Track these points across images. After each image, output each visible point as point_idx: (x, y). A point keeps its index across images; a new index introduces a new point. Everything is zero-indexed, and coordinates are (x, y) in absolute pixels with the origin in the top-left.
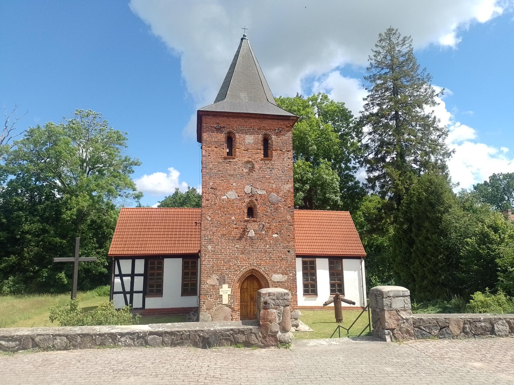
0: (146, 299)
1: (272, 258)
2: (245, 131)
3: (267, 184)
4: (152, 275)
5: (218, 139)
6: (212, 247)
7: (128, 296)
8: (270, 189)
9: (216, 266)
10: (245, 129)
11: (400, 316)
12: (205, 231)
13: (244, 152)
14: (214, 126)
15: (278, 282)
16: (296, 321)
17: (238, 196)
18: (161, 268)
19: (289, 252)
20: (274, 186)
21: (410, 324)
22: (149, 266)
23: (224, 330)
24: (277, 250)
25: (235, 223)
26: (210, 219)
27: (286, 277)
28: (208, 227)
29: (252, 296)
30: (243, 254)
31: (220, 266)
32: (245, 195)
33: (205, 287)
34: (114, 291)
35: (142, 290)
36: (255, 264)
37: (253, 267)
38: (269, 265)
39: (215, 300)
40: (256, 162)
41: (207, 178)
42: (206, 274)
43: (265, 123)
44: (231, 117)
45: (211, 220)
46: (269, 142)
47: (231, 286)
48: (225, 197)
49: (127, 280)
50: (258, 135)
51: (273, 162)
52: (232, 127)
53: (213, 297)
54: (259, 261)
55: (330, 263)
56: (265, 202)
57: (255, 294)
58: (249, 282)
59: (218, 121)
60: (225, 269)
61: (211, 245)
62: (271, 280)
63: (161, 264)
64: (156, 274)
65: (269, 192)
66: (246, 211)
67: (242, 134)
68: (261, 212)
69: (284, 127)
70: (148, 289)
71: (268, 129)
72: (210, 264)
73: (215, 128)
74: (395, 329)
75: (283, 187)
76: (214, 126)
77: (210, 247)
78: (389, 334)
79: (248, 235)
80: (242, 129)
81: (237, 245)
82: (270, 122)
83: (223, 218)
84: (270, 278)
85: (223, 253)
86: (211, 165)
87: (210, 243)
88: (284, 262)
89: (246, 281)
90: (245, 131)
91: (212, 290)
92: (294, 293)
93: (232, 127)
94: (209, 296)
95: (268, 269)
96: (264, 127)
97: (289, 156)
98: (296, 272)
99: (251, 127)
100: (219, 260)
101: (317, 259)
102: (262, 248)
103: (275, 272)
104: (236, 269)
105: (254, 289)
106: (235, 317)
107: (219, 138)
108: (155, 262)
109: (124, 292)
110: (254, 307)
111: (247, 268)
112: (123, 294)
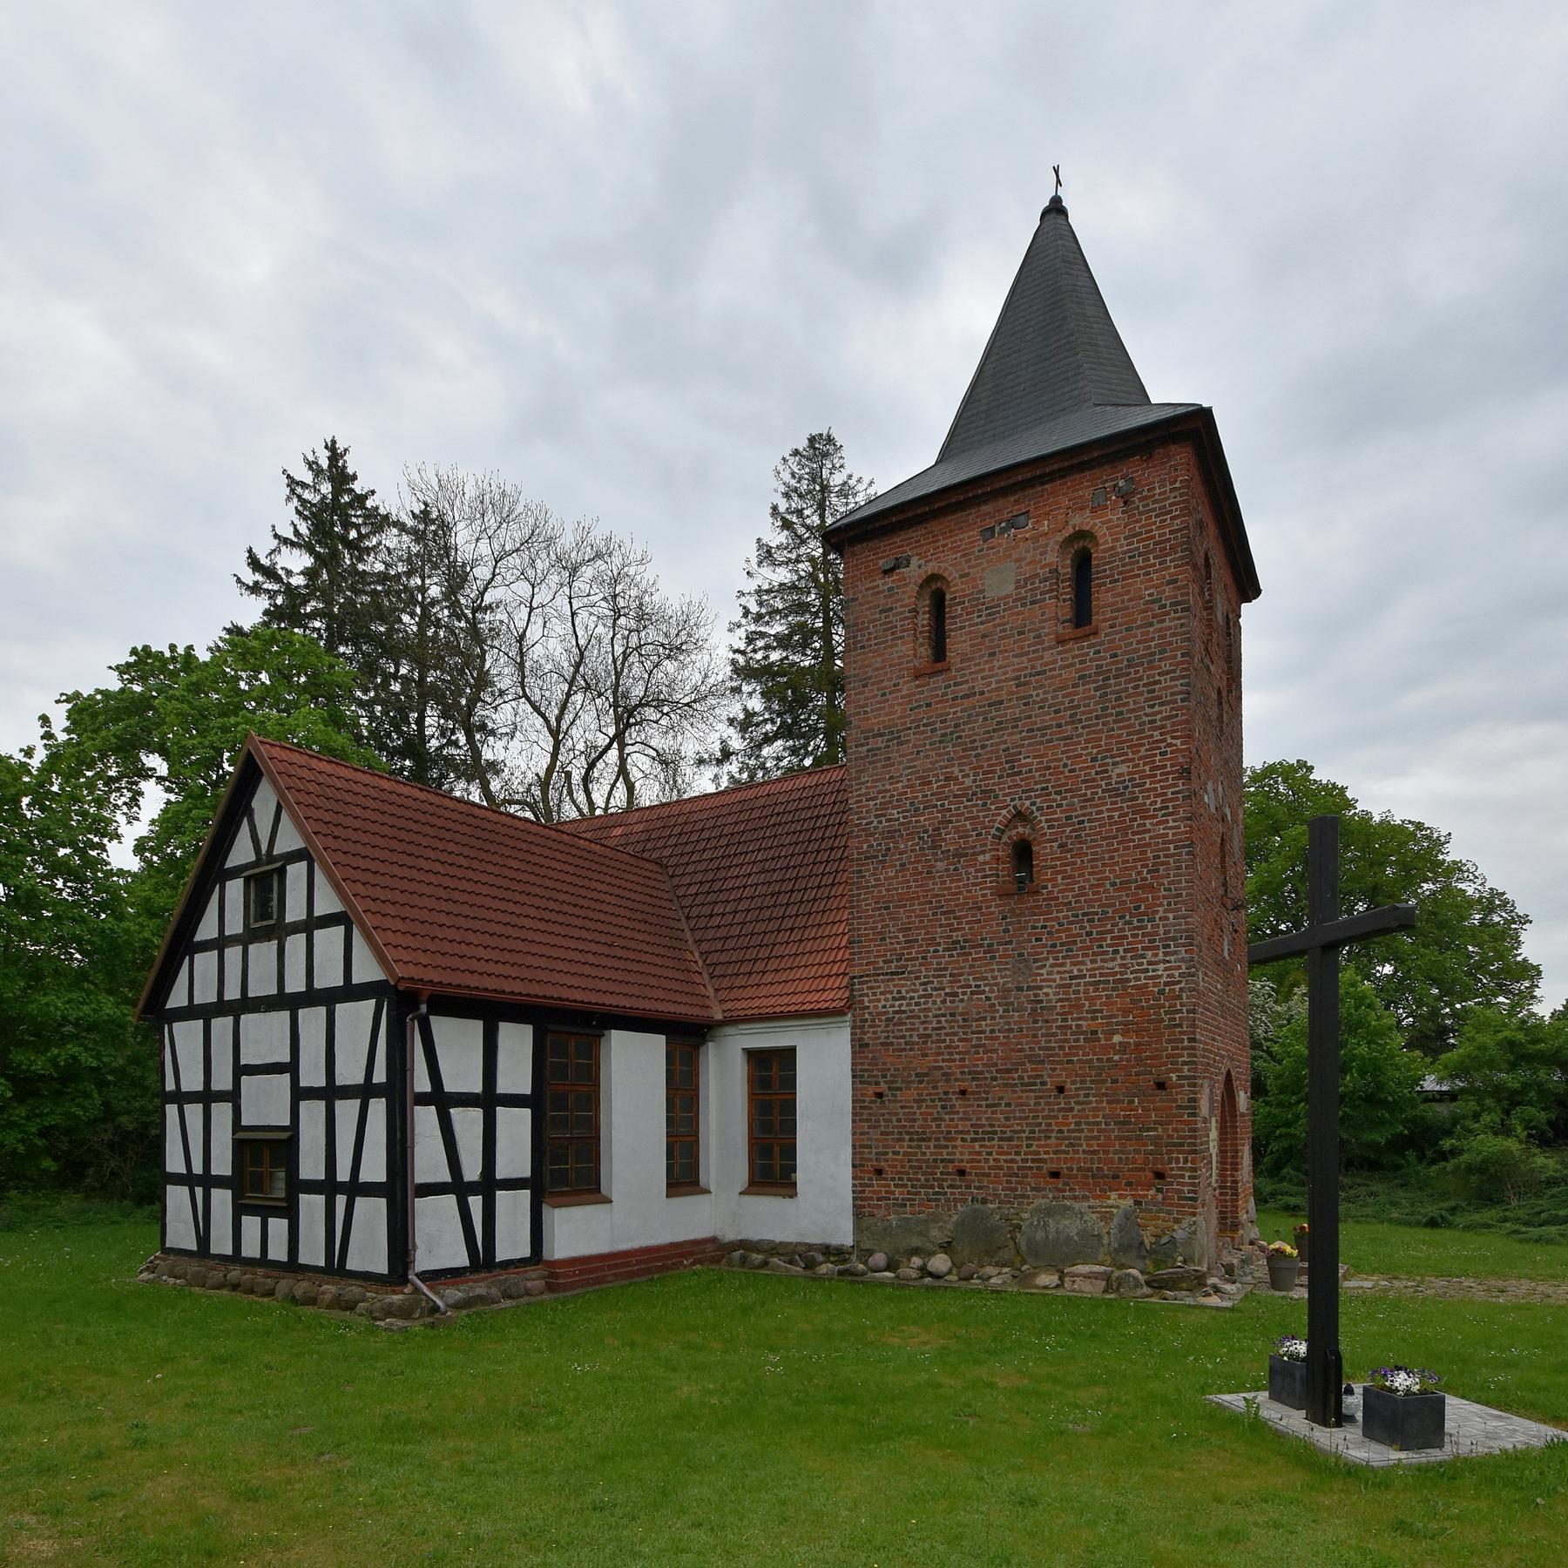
7: (476, 1203)
49: (468, 1122)
109: (458, 1187)
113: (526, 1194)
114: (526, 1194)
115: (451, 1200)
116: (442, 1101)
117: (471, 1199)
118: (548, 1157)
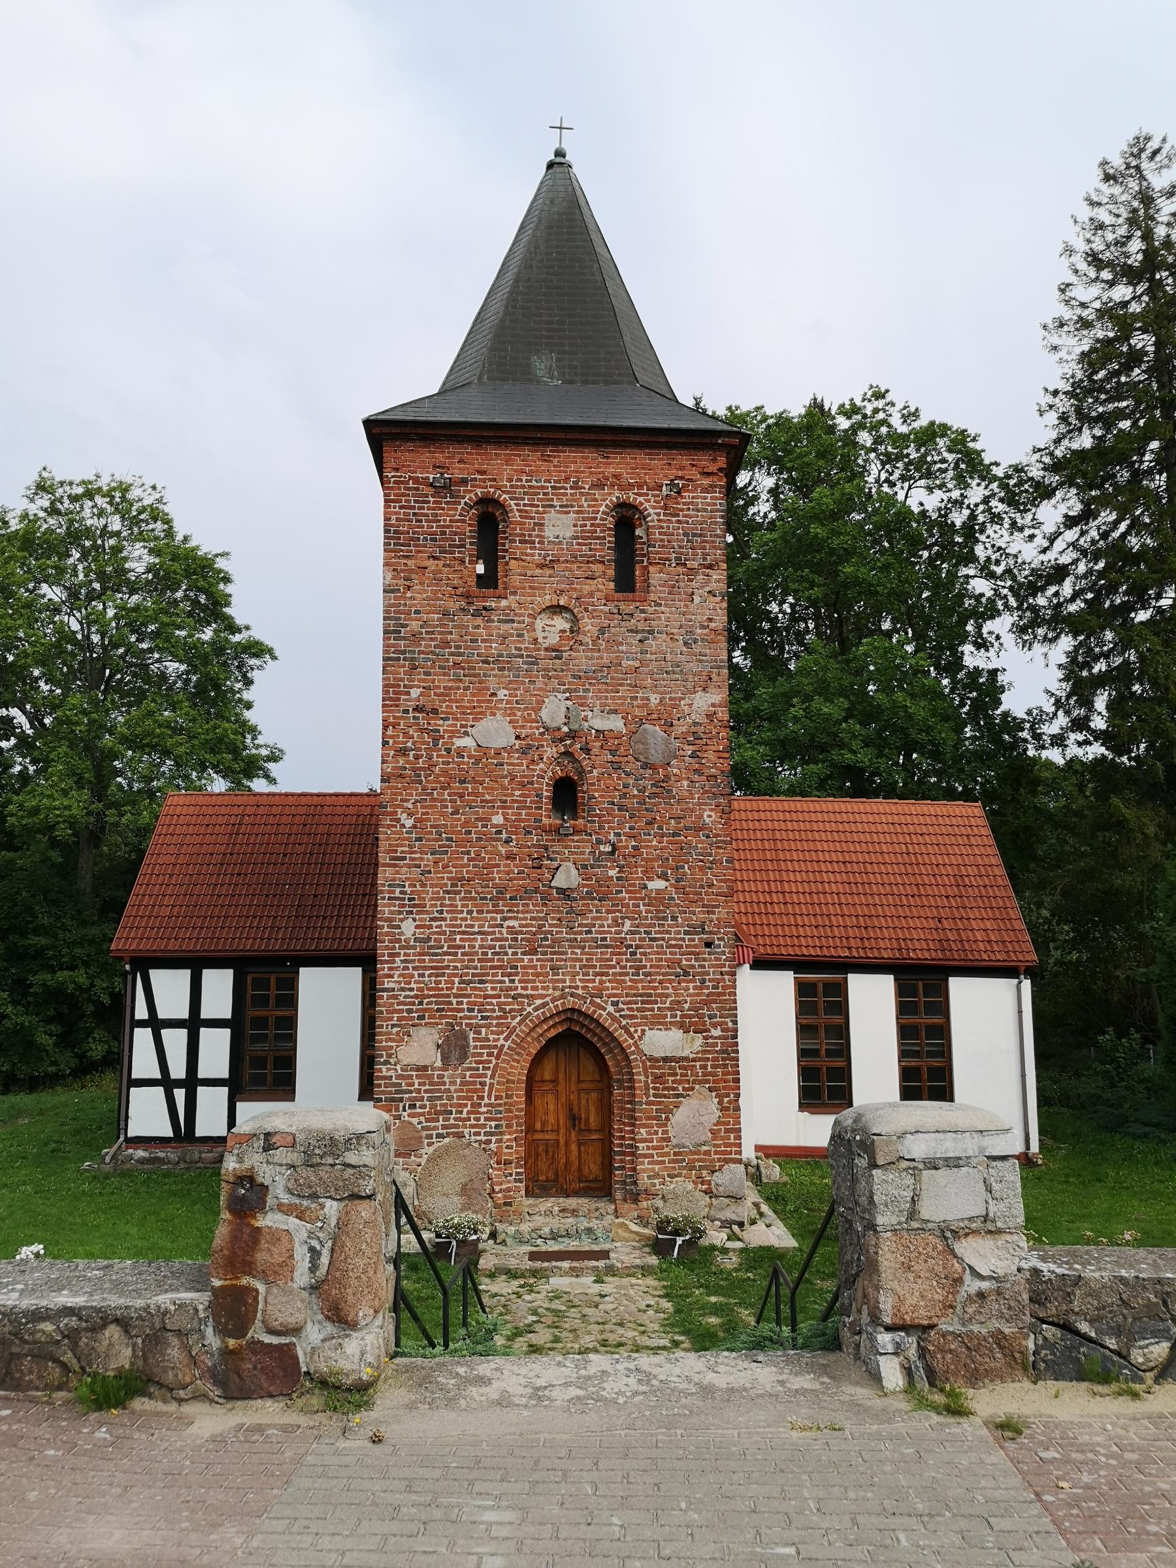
0: (240, 1106)
1: (645, 967)
2: (544, 494)
3: (623, 691)
4: (261, 1023)
5: (443, 526)
6: (417, 927)
7: (180, 1094)
8: (637, 712)
9: (432, 996)
10: (543, 487)
11: (960, 1260)
12: (395, 866)
13: (538, 571)
14: (428, 478)
15: (666, 1059)
16: (733, 1207)
17: (518, 737)
18: (290, 1000)
19: (708, 945)
20: (654, 699)
21: (1013, 1304)
22: (250, 992)
23: (25, 1313)
24: (663, 939)
25: (504, 836)
26: (409, 823)
27: (699, 1040)
28: (402, 852)
29: (576, 1109)
30: (533, 952)
31: (448, 996)
32: (542, 734)
33: (392, 1073)
34: (134, 1076)
35: (225, 1074)
36: (580, 992)
37: (570, 1002)
38: (635, 995)
39: (427, 1120)
40: (586, 610)
41: (402, 670)
42: (393, 1026)
43: (619, 463)
44: (489, 443)
45: (414, 827)
46: (638, 532)
47: (490, 1073)
48: (466, 742)
49: (175, 1040)
50: (593, 506)
51: (651, 610)
52: (495, 480)
53: (419, 1110)
54: (593, 981)
55: (902, 991)
56: (620, 759)
57: (583, 1102)
58: (562, 1055)
59: (440, 457)
60: (465, 1006)
61: (414, 920)
62: (640, 1052)
63: (290, 986)
64: (272, 1021)
65: (636, 724)
66: (545, 794)
67: (531, 505)
68: (601, 796)
69: (693, 473)
70: (247, 1072)
71: (631, 486)
72: (411, 990)
73: (431, 485)
74: (932, 1327)
75: (687, 701)
76: (428, 478)
77: (408, 928)
78: (898, 1351)
79: (553, 884)
80: (530, 487)
81: (510, 918)
82: (641, 457)
83: (459, 819)
84: (635, 1044)
85: (459, 947)
86: (414, 623)
87: (411, 912)
88: (691, 985)
89: (552, 1055)
90: (544, 494)
91: (416, 1086)
92: (729, 1102)
93: (495, 480)
94: (404, 1107)
95: (631, 1009)
96: (615, 476)
97: (713, 586)
98: (735, 1022)
99: (567, 479)
100: (443, 975)
101: (850, 976)
102: (604, 932)
103: (658, 1022)
104: (508, 1008)
105: (579, 1081)
106: (504, 1187)
107: (445, 521)
108: (916, 987)
109: (166, 1082)
110: (579, 1151)
111: (547, 1004)
112: (161, 1089)
113: (225, 1090)
114: (225, 1090)
115: (160, 1091)
116: (156, 1024)
117: (176, 1091)
118: (247, 1064)
